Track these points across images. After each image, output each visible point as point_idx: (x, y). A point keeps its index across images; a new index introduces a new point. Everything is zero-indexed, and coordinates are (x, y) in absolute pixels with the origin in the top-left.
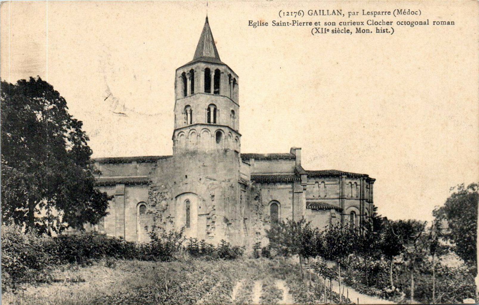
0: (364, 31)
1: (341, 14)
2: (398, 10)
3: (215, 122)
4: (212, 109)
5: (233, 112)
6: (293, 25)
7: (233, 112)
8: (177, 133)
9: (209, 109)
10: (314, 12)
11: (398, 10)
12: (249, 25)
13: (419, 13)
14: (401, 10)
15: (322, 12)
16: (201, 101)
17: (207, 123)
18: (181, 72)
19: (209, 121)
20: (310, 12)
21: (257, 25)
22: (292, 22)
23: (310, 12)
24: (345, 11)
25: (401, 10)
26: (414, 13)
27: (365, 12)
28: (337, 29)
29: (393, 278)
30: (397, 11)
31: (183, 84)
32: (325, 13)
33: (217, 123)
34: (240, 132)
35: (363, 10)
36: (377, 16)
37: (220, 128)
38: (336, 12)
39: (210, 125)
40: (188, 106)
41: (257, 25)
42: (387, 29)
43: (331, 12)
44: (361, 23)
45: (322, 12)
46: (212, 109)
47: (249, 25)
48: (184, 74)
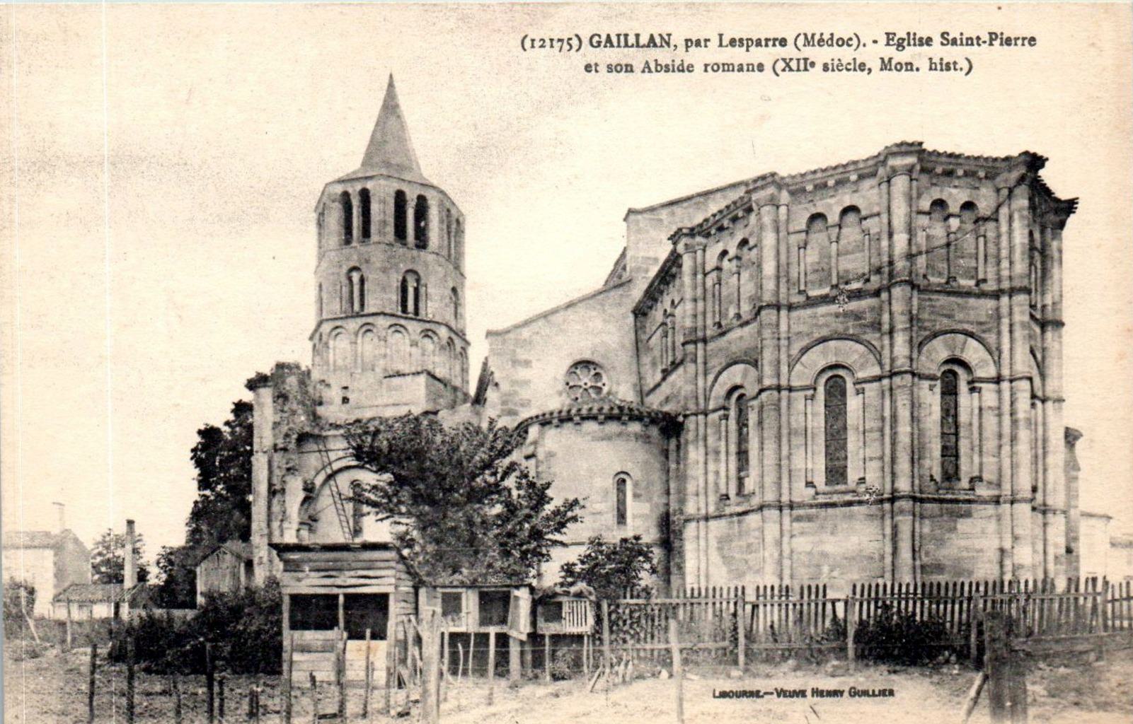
0: (899, 67)
1: (668, 44)
2: (806, 35)
3: (417, 312)
4: (356, 276)
5: (454, 290)
6: (991, 44)
7: (454, 290)
8: (326, 328)
9: (404, 281)
10: (604, 38)
11: (806, 35)
12: (888, 44)
13: (855, 42)
14: (813, 35)
15: (622, 38)
16: (380, 257)
17: (400, 313)
18: (339, 189)
19: (404, 310)
20: (596, 39)
21: (905, 43)
22: (987, 38)
23: (596, 39)
24: (677, 39)
25: (813, 35)
26: (842, 42)
27: (726, 41)
28: (836, 62)
29: (746, 655)
30: (802, 37)
31: (343, 214)
32: (632, 40)
33: (422, 315)
34: (468, 338)
35: (721, 35)
36: (753, 49)
37: (428, 326)
38: (658, 40)
39: (406, 318)
40: (355, 269)
41: (905, 43)
42: (955, 63)
43: (644, 40)
44: (794, 65)
45: (622, 38)
46: (356, 276)
47: (888, 44)
48: (346, 195)
